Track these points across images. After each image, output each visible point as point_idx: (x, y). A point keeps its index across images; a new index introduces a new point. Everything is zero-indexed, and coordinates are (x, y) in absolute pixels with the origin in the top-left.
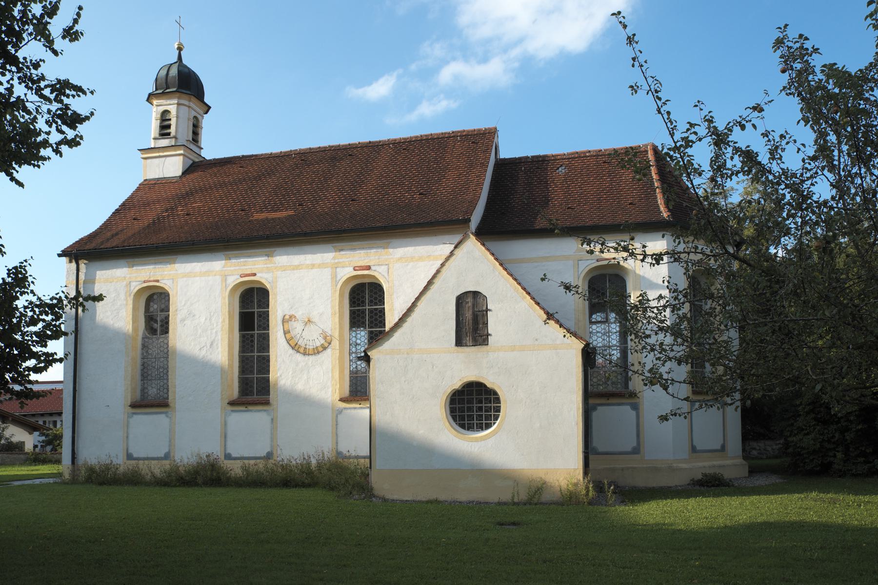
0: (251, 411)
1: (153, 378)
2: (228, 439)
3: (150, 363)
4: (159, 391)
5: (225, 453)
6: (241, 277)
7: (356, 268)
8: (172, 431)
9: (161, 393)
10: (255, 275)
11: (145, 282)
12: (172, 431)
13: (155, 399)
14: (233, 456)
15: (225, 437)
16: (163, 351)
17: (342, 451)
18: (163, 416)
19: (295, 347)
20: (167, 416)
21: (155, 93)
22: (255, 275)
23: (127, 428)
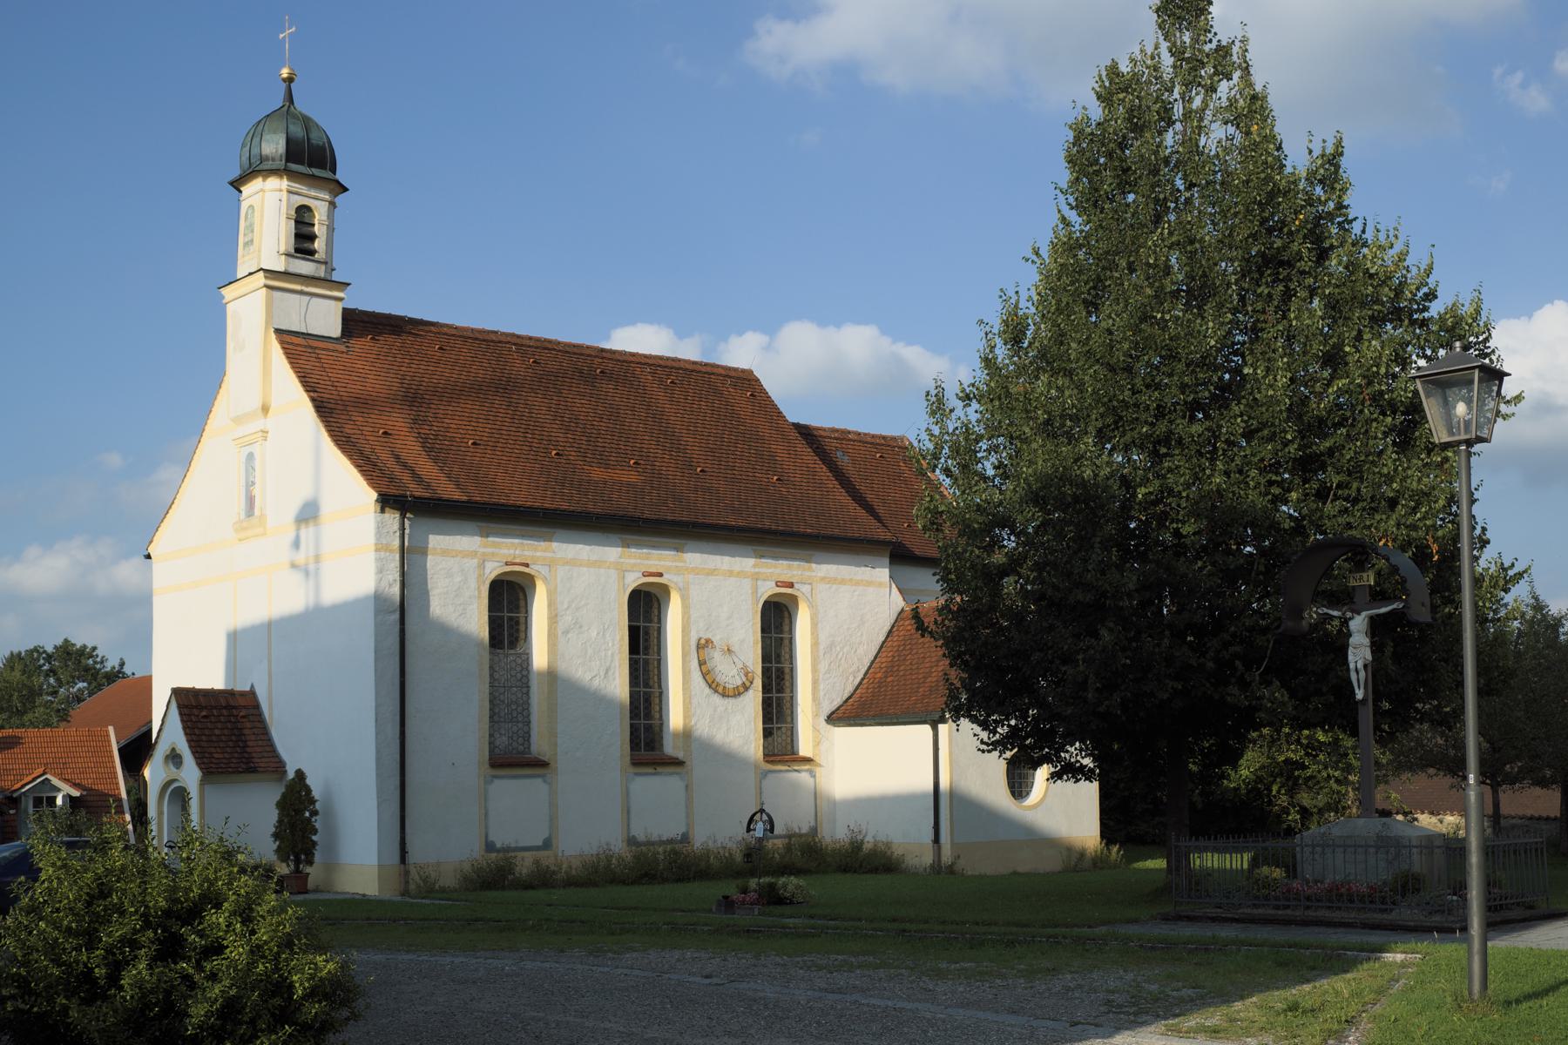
6: (777, 586)
10: (661, 575)
11: (507, 564)
15: (628, 812)
19: (713, 685)
20: (545, 781)
22: (661, 575)
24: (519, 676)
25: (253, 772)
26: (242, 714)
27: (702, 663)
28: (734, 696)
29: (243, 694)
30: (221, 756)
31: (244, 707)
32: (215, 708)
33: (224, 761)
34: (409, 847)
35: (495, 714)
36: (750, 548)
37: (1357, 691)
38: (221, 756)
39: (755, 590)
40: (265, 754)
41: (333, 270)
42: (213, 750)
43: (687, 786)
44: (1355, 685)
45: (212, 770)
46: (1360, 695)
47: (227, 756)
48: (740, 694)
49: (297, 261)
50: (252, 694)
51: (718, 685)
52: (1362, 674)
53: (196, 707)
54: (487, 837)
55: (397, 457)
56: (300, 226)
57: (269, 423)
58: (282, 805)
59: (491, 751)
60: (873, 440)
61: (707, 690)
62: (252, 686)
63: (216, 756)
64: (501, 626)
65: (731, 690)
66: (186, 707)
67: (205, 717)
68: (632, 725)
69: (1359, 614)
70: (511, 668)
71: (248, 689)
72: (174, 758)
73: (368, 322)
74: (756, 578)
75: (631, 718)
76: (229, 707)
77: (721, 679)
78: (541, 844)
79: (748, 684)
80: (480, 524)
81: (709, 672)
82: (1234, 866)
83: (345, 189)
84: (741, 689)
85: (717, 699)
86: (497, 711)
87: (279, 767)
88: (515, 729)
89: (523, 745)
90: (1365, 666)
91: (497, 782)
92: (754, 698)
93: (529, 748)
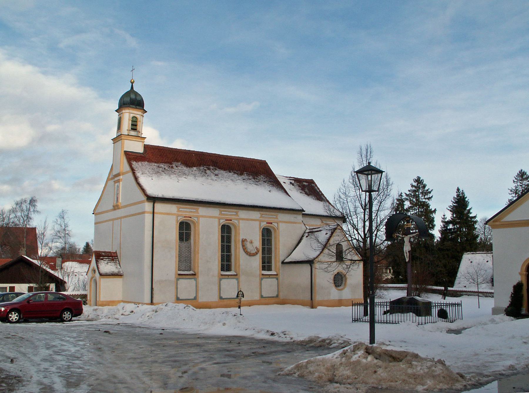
6: (267, 223)
11: (185, 217)
27: (243, 246)
28: (253, 256)
29: (114, 253)
37: (406, 259)
39: (260, 225)
41: (142, 134)
44: (406, 257)
46: (407, 260)
51: (248, 252)
52: (408, 254)
61: (245, 254)
62: (116, 251)
68: (222, 264)
69: (407, 235)
71: (115, 252)
74: (261, 221)
77: (249, 251)
78: (221, 296)
81: (245, 248)
82: (356, 307)
83: (146, 112)
85: (248, 257)
90: (409, 252)
92: (259, 257)
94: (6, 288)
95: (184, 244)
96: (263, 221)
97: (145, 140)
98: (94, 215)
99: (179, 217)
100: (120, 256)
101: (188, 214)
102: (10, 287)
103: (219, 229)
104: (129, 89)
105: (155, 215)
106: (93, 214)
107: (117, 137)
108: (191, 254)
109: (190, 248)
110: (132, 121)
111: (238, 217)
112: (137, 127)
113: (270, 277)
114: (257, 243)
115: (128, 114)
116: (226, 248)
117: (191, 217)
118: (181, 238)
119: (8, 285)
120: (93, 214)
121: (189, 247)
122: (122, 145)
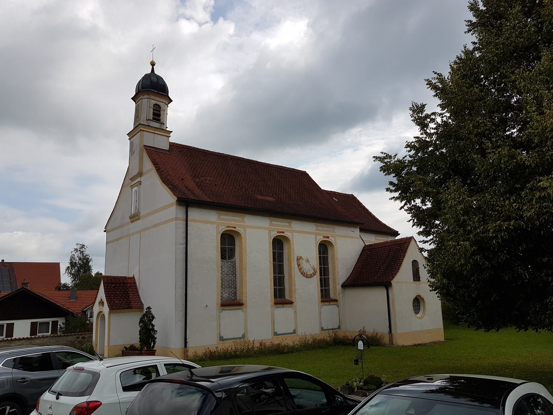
0: (285, 307)
1: (226, 287)
2: (275, 323)
3: (224, 277)
4: (229, 295)
5: (274, 332)
6: (324, 238)
7: (324, 237)
8: (246, 321)
9: (231, 296)
10: (284, 233)
11: (227, 227)
12: (246, 321)
13: (227, 300)
14: (224, 338)
15: (274, 322)
16: (231, 270)
17: (132, 343)
18: (240, 311)
19: (303, 274)
20: (242, 311)
21: (141, 90)
22: (284, 233)
23: (219, 319)
24: (232, 270)
25: (130, 308)
26: (128, 286)
27: (299, 265)
28: (310, 277)
29: (130, 278)
30: (118, 302)
31: (130, 283)
32: (118, 283)
33: (119, 304)
34: (188, 340)
35: (223, 285)
36: (314, 224)
38: (118, 302)
39: (316, 238)
40: (136, 301)
42: (115, 300)
43: (295, 311)
45: (113, 307)
47: (120, 302)
48: (312, 277)
49: (153, 122)
50: (133, 278)
51: (304, 273)
53: (111, 283)
54: (220, 334)
55: (187, 187)
56: (154, 111)
57: (142, 179)
58: (141, 321)
59: (222, 299)
60: (343, 195)
61: (301, 276)
63: (116, 302)
64: (225, 251)
65: (309, 275)
66: (106, 283)
67: (113, 287)
70: (229, 267)
72: (102, 303)
73: (179, 147)
75: (274, 286)
76: (124, 283)
77: (305, 271)
78: (292, 332)
79: (313, 275)
80: (217, 211)
84: (313, 275)
85: (304, 279)
86: (224, 284)
87: (140, 306)
88: (231, 291)
89: (234, 297)
91: (224, 312)
92: (317, 278)
93: (236, 298)
94: (49, 322)
95: (228, 263)
96: (319, 234)
97: (170, 135)
98: (106, 233)
99: (220, 227)
100: (139, 283)
101: (232, 224)
102: (52, 321)
103: (269, 243)
104: (149, 71)
105: (188, 223)
106: (105, 231)
107: (134, 129)
108: (235, 277)
109: (234, 269)
110: (153, 109)
111: (292, 229)
112: (160, 118)
113: (330, 304)
114: (315, 262)
115: (148, 102)
116: (278, 268)
117: (235, 228)
118: (223, 257)
119: (50, 320)
120: (105, 231)
121: (234, 266)
122: (141, 138)
